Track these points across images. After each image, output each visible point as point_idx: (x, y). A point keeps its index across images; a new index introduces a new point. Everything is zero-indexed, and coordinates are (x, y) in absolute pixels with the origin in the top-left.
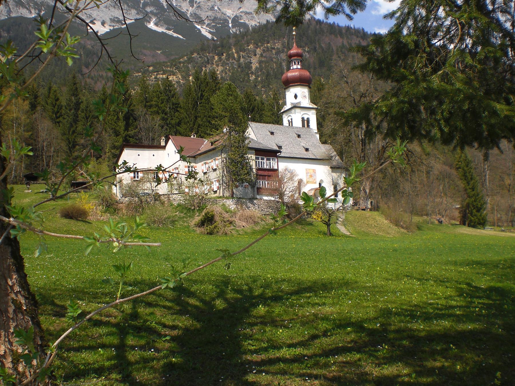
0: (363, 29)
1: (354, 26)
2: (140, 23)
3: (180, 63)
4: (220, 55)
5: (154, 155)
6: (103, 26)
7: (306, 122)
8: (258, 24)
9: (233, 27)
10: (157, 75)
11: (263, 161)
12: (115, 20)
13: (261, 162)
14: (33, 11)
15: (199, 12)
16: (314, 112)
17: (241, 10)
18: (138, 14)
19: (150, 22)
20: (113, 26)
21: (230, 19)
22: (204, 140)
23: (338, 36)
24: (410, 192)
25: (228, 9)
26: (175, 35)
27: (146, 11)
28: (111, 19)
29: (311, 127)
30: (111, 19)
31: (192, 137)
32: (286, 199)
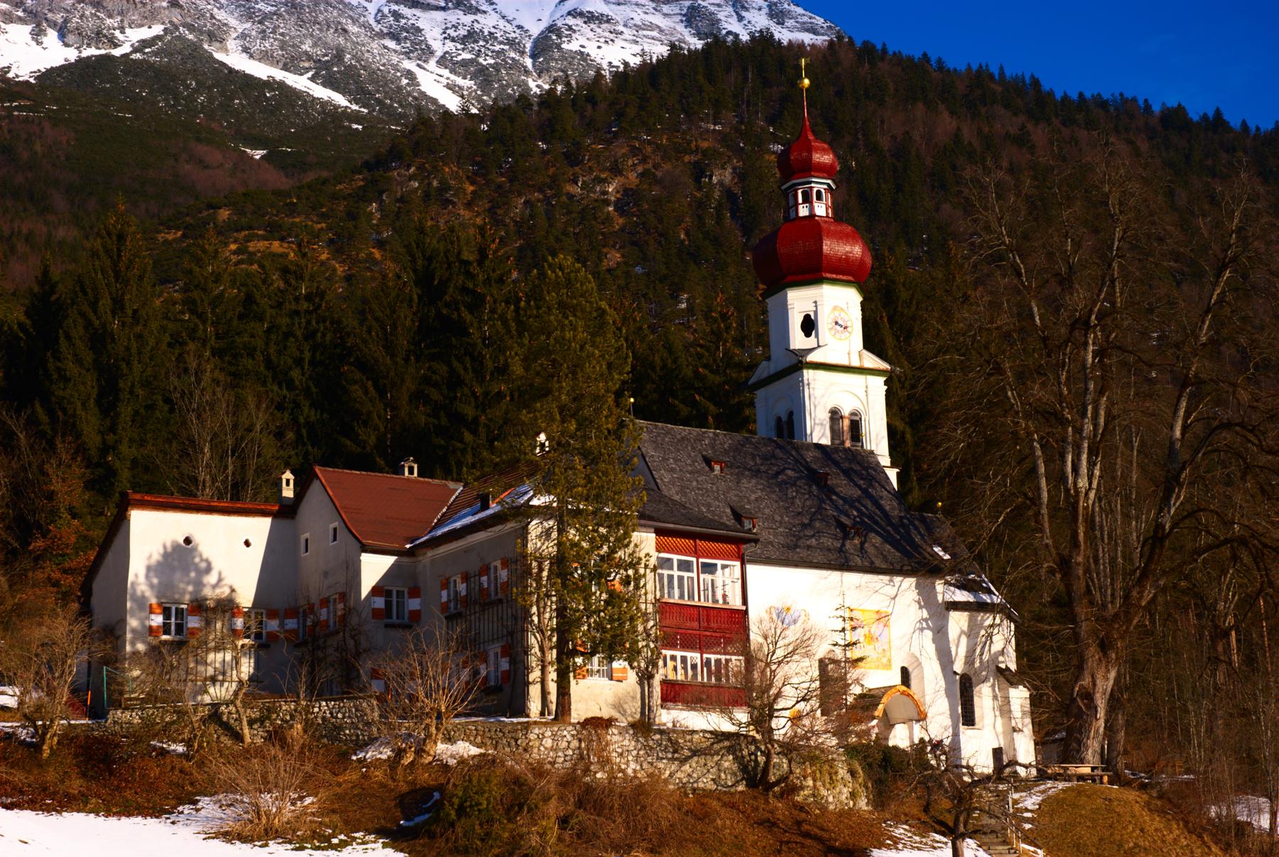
0: (1036, 82)
1: (1002, 68)
8: (638, 60)
10: (248, 239)
11: (686, 575)
13: (681, 579)
16: (882, 380)
22: (451, 485)
23: (941, 107)
32: (781, 727)
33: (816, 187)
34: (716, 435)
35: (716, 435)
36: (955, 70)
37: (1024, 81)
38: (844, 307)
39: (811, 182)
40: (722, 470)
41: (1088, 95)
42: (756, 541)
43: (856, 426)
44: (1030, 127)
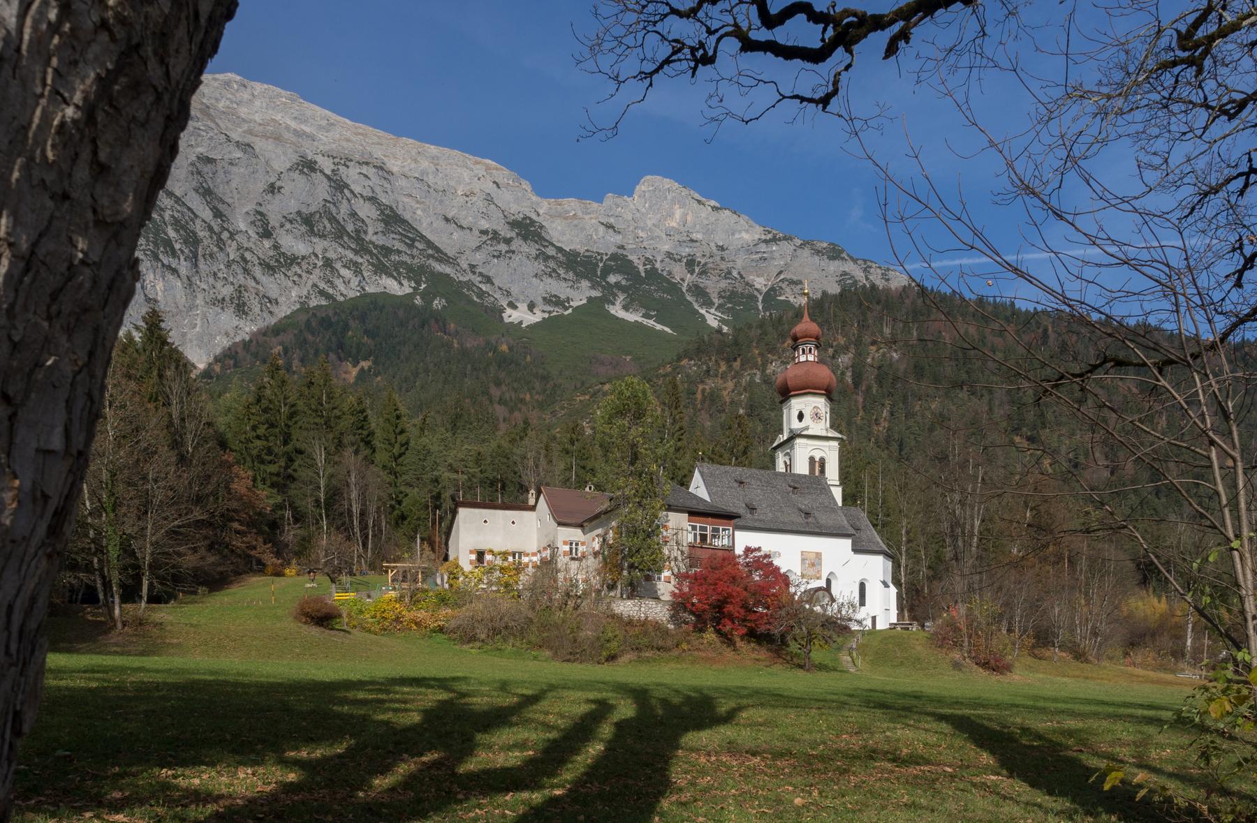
2: (595, 307)
3: (657, 377)
4: (729, 360)
5: (513, 523)
6: (532, 311)
7: (817, 465)
9: (765, 309)
12: (551, 301)
14: (405, 282)
15: (703, 282)
16: (835, 444)
17: (782, 277)
18: (593, 287)
19: (613, 304)
20: (550, 312)
21: (761, 294)
24: (487, 403)
25: (758, 276)
26: (659, 327)
27: (607, 283)
28: (544, 299)
29: (827, 475)
30: (544, 299)
31: (587, 489)
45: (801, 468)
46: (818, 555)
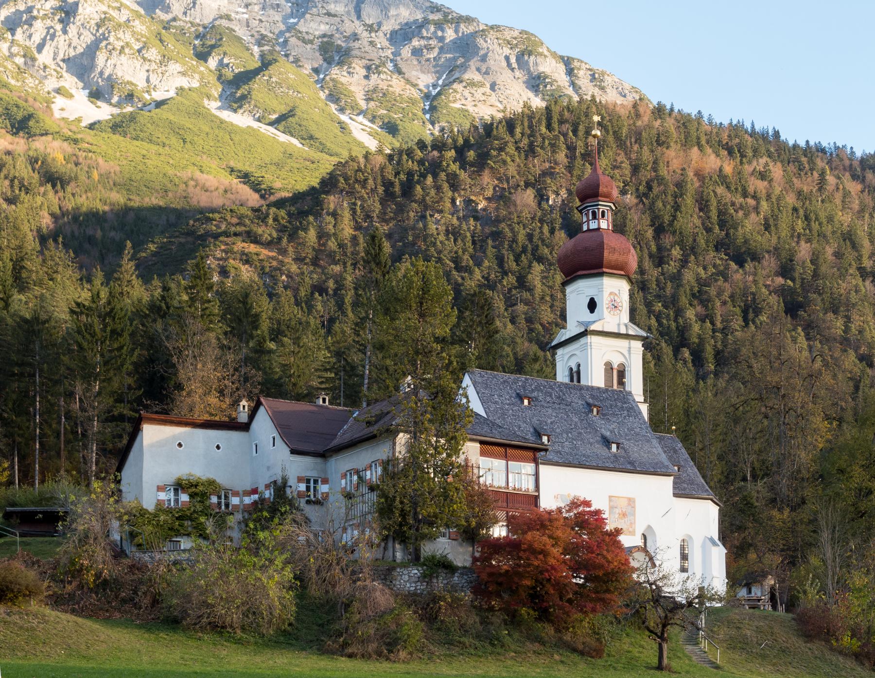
0: (777, 134)
33: (602, 208)
34: (526, 379)
35: (526, 379)
36: (721, 124)
37: (768, 133)
38: (617, 292)
39: (598, 205)
40: (529, 403)
41: (812, 143)
42: (546, 450)
43: (622, 374)
44: (771, 164)
45: (595, 378)
46: (631, 501)
